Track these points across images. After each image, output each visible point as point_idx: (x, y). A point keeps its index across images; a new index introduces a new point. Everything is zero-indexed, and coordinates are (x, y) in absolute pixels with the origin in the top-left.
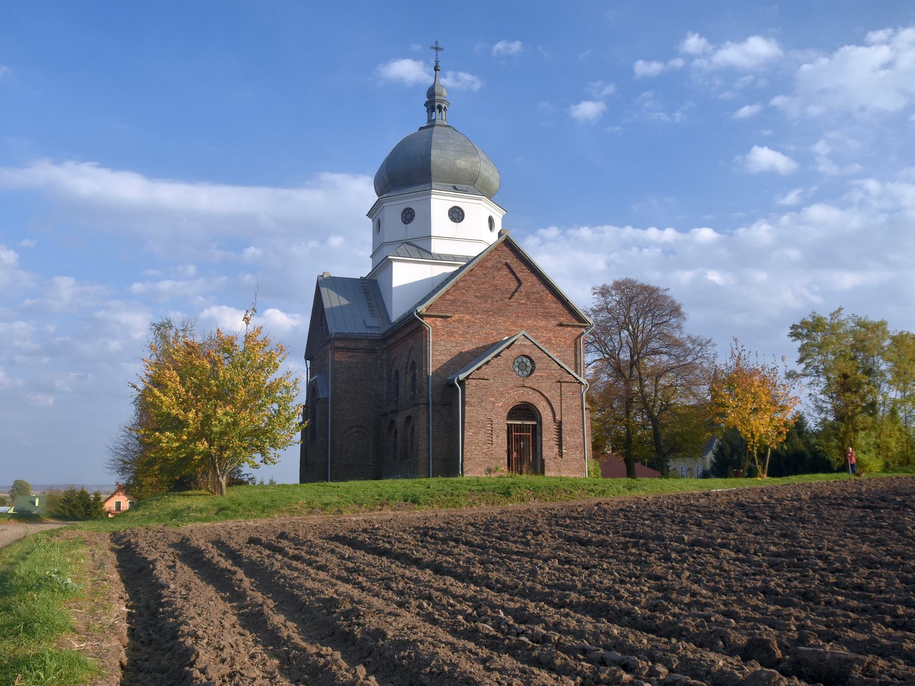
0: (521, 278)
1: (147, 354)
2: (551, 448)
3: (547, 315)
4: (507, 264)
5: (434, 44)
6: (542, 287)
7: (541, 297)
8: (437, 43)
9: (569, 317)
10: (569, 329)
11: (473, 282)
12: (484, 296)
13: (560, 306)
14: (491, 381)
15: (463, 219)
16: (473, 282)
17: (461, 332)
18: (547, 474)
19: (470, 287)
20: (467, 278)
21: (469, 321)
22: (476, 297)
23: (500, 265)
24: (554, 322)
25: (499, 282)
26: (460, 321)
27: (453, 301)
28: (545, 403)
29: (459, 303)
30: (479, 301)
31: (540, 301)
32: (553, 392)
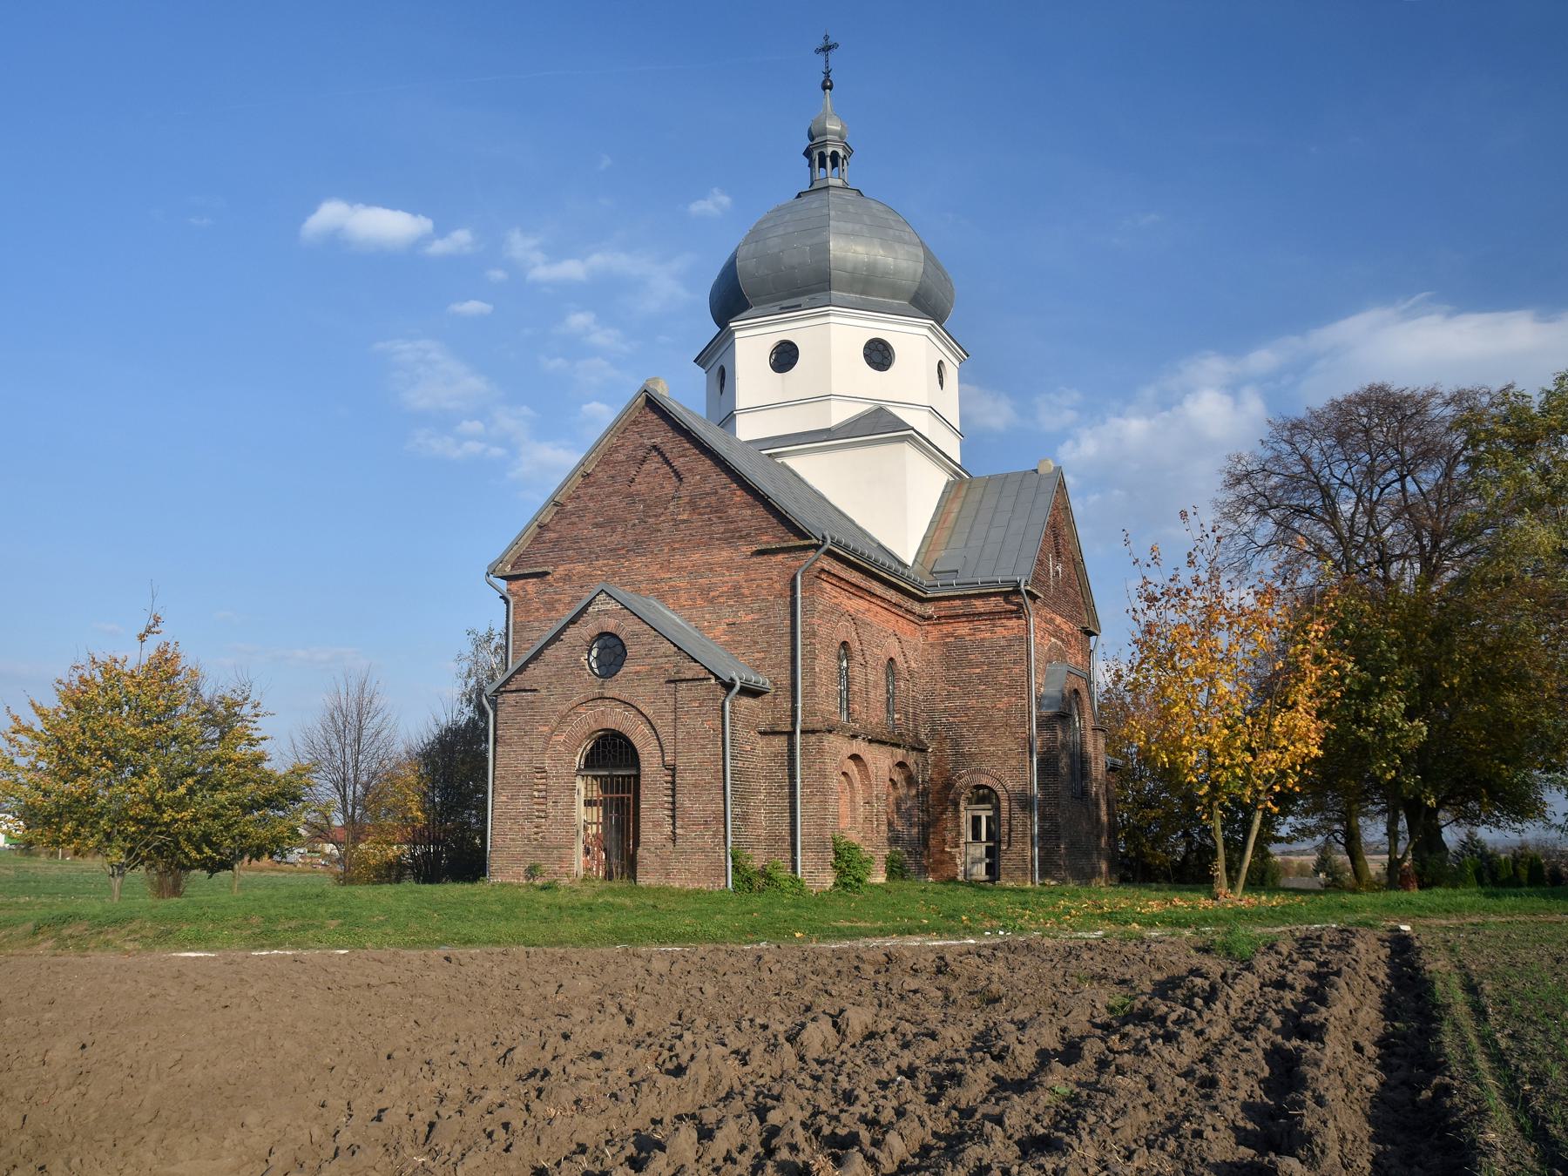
0: (681, 469)
1: (51, 702)
2: (657, 824)
3: (733, 537)
4: (655, 447)
5: (820, 43)
6: (724, 479)
7: (721, 500)
8: (826, 38)
9: (781, 530)
10: (780, 557)
11: (592, 498)
12: (610, 521)
13: (760, 511)
14: (544, 692)
15: (865, 356)
16: (592, 498)
17: (568, 599)
18: (644, 880)
19: (586, 508)
20: (581, 492)
21: (582, 576)
22: (597, 525)
23: (641, 453)
24: (747, 549)
25: (643, 488)
26: (567, 578)
27: (556, 542)
28: (647, 730)
29: (566, 545)
30: (601, 532)
31: (719, 510)
32: (660, 704)
